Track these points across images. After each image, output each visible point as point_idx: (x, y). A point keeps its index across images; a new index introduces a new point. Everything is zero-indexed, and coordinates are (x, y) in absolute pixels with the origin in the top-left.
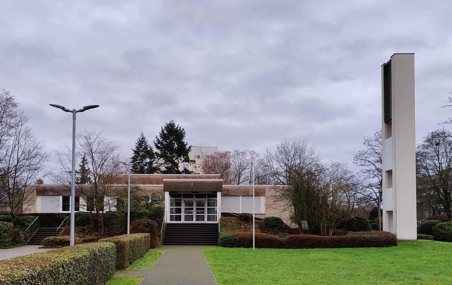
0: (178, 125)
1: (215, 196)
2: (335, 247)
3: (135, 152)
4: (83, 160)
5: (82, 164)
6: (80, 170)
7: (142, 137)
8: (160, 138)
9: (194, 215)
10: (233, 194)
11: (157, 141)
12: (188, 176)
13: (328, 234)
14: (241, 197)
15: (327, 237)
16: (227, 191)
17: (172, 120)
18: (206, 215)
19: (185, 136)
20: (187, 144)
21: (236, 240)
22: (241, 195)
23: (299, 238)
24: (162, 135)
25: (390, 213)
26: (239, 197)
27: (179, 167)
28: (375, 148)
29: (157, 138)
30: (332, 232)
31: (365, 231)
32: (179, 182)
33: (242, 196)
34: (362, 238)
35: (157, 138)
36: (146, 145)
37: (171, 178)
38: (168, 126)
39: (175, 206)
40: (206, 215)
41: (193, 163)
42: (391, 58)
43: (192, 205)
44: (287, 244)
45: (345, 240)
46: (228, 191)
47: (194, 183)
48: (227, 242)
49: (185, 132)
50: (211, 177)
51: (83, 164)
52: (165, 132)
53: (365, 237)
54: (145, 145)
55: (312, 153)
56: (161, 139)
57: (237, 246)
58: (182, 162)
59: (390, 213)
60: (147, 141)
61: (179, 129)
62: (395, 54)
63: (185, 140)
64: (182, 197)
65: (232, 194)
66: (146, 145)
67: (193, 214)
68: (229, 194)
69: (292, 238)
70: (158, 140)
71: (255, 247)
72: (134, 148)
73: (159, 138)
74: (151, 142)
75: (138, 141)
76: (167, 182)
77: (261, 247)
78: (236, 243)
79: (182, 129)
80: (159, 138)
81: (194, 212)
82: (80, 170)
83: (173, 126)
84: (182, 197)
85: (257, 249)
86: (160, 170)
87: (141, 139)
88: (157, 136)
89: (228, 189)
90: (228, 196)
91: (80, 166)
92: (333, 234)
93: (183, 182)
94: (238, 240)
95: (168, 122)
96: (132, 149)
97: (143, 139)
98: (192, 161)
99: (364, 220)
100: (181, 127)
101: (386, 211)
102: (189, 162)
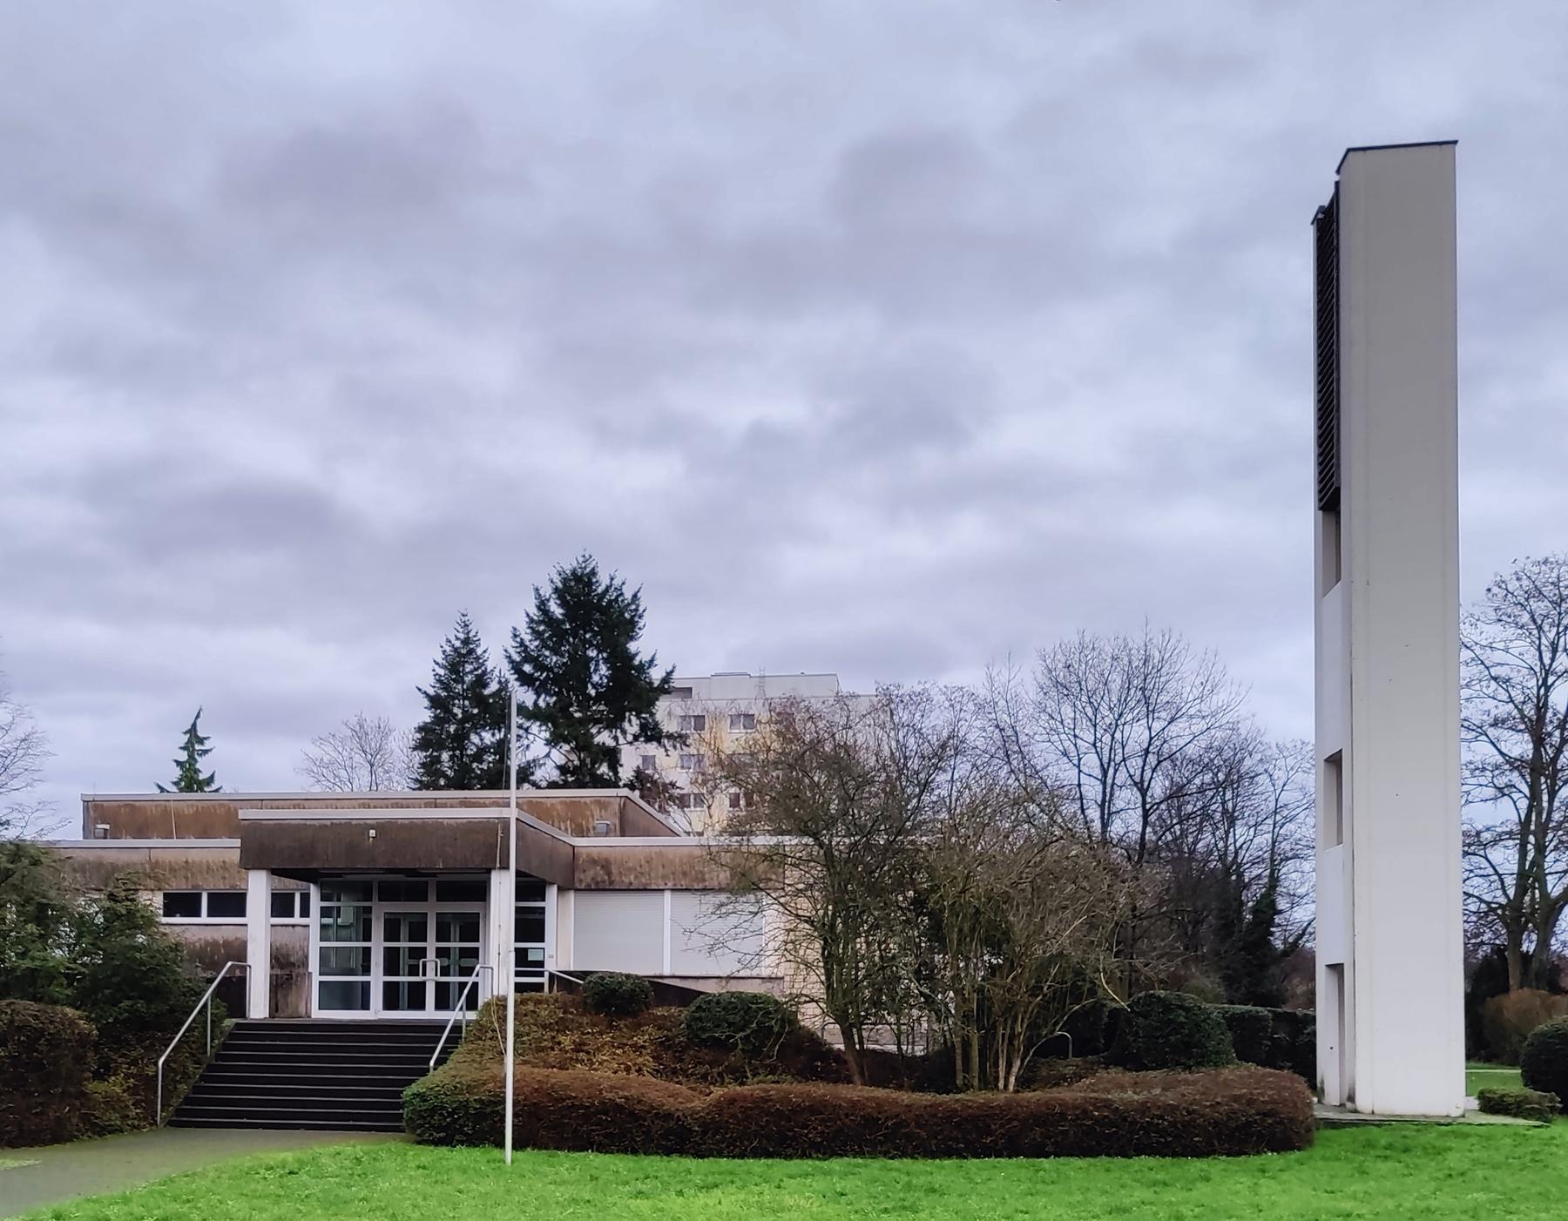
0: (612, 579)
1: (481, 892)
2: (948, 1153)
3: (435, 702)
4: (189, 741)
5: (183, 756)
6: (175, 784)
7: (462, 636)
8: (530, 637)
9: (427, 983)
10: (631, 884)
11: (518, 650)
12: (583, 800)
13: (989, 1082)
14: (668, 895)
15: (982, 1097)
16: (603, 867)
17: (587, 556)
18: (377, 979)
19: (641, 625)
20: (652, 661)
21: (465, 1105)
22: (670, 885)
23: (771, 1100)
24: (539, 623)
25: (1337, 969)
26: (659, 894)
27: (621, 766)
28: (1488, 656)
29: (518, 639)
30: (1015, 1070)
31: (1189, 1068)
32: (312, 822)
33: (672, 890)
34: (1097, 1109)
35: (515, 636)
36: (480, 671)
37: (428, 805)
38: (565, 581)
39: (458, 939)
40: (431, 979)
41: (678, 745)
42: (1338, 172)
43: (418, 933)
44: (704, 1133)
45: (1002, 1119)
46: (606, 865)
47: (383, 827)
48: (424, 1118)
49: (641, 609)
50: (585, 803)
51: (191, 757)
52: (557, 610)
53: (1107, 1104)
54: (476, 669)
55: (1209, 687)
56: (536, 639)
57: (466, 1141)
58: (631, 743)
59: (1337, 969)
60: (485, 652)
61: (618, 596)
62: (1349, 150)
63: (641, 647)
64: (375, 896)
65: (627, 881)
66: (480, 671)
67: (424, 974)
68: (611, 882)
69: (732, 1101)
70: (522, 643)
71: (514, 1147)
72: (429, 684)
73: (527, 638)
74: (496, 655)
75: (444, 652)
76: (255, 825)
77: (539, 1145)
78: (462, 1126)
79: (628, 596)
80: (527, 637)
81: (430, 968)
82: (175, 784)
83: (590, 584)
84: (375, 896)
85: (529, 1155)
86: (531, 778)
87: (458, 644)
88: (515, 629)
89: (607, 860)
90: (604, 890)
91: (178, 763)
92: (1025, 1083)
93: (328, 822)
94: (475, 1109)
95: (568, 569)
96: (420, 690)
97: (466, 642)
98: (670, 736)
99: (1187, 1010)
100: (623, 584)
101: (1328, 966)
102: (659, 743)
